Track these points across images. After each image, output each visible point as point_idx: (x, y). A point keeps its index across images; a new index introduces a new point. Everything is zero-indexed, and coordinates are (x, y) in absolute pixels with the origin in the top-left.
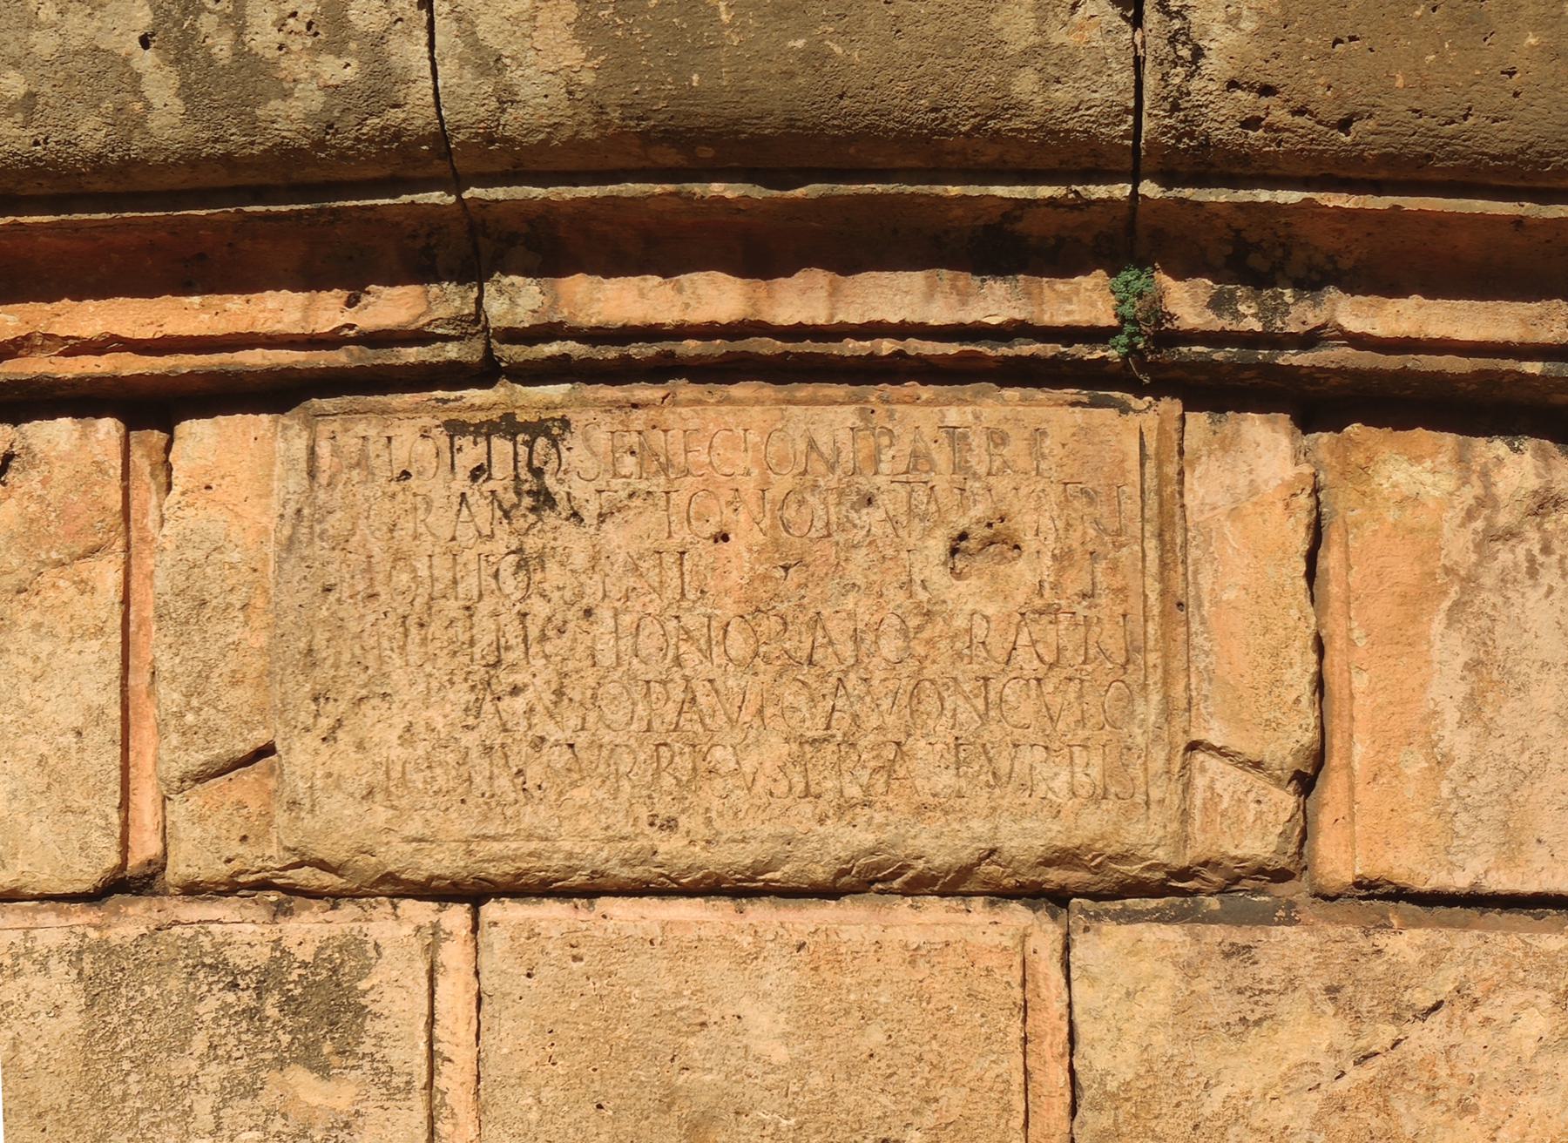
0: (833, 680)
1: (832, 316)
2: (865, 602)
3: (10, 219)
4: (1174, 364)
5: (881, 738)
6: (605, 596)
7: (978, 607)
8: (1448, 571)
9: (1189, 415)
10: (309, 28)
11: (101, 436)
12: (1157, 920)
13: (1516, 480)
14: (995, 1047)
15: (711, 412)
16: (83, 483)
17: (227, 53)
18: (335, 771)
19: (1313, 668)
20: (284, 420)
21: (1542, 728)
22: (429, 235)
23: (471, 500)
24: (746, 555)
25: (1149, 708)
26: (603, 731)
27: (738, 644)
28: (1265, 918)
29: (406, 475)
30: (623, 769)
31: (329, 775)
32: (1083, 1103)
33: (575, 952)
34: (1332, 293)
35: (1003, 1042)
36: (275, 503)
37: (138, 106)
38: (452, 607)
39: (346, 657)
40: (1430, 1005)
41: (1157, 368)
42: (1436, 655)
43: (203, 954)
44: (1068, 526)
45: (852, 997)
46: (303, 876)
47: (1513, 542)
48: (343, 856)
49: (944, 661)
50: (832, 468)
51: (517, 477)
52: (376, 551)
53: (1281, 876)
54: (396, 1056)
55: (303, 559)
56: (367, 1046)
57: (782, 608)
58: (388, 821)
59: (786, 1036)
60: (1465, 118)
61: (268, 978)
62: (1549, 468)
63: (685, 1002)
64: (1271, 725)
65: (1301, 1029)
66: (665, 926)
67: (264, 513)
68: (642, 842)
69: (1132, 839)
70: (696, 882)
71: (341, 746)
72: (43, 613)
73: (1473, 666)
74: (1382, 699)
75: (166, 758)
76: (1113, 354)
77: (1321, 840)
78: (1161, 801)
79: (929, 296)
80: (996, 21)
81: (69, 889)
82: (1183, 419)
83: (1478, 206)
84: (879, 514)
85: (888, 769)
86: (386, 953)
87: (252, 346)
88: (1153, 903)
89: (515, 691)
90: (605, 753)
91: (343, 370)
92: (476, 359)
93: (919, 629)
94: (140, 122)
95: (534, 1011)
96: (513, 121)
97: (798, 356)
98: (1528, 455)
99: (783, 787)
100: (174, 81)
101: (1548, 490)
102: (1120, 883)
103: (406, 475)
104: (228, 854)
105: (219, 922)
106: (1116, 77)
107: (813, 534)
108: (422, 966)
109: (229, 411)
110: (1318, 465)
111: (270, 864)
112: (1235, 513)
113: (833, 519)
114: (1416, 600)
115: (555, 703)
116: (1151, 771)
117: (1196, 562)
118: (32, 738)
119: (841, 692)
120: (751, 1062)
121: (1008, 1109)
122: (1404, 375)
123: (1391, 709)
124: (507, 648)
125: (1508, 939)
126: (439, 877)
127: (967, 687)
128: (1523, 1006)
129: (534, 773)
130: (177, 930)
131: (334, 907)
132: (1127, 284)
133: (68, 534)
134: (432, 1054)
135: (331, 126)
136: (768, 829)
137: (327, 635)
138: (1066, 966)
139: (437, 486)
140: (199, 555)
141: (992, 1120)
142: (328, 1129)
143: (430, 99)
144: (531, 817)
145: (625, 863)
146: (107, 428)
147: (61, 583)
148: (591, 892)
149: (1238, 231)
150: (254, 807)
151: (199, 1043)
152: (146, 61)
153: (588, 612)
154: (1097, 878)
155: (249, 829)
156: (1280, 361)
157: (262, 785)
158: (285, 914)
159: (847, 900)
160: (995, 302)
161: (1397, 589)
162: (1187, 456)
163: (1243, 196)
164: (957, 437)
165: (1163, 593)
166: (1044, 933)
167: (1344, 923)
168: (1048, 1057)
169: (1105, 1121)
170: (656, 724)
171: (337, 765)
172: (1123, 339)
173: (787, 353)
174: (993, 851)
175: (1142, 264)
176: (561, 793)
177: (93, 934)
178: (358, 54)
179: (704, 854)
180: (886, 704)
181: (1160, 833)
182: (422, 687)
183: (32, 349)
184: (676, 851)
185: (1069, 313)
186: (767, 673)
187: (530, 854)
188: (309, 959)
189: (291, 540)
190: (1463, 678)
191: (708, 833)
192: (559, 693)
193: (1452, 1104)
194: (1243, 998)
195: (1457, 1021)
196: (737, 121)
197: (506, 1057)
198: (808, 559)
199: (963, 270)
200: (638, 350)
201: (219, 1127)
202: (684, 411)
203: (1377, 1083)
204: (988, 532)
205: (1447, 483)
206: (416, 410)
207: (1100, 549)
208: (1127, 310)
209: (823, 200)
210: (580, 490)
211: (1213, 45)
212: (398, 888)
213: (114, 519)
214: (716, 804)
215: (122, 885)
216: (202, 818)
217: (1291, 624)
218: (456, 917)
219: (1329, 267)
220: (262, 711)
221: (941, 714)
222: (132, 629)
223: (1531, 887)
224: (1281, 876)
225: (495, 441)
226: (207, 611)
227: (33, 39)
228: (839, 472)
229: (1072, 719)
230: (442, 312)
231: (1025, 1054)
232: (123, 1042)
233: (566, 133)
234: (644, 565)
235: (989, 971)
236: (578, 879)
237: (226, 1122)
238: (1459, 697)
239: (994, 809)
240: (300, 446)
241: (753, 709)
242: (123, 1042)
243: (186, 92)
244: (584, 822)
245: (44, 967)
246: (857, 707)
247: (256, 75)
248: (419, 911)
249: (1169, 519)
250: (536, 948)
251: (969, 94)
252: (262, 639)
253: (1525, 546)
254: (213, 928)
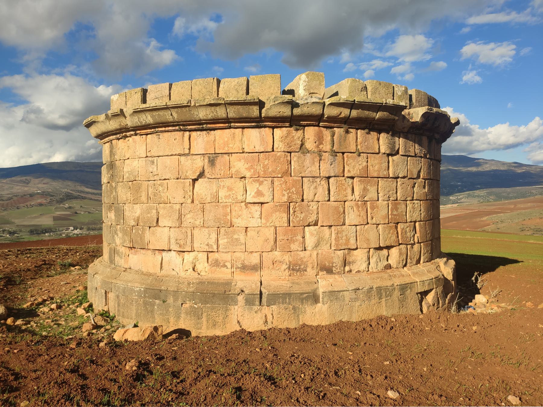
41: (181, 130)
160: (174, 128)
215: (147, 157)
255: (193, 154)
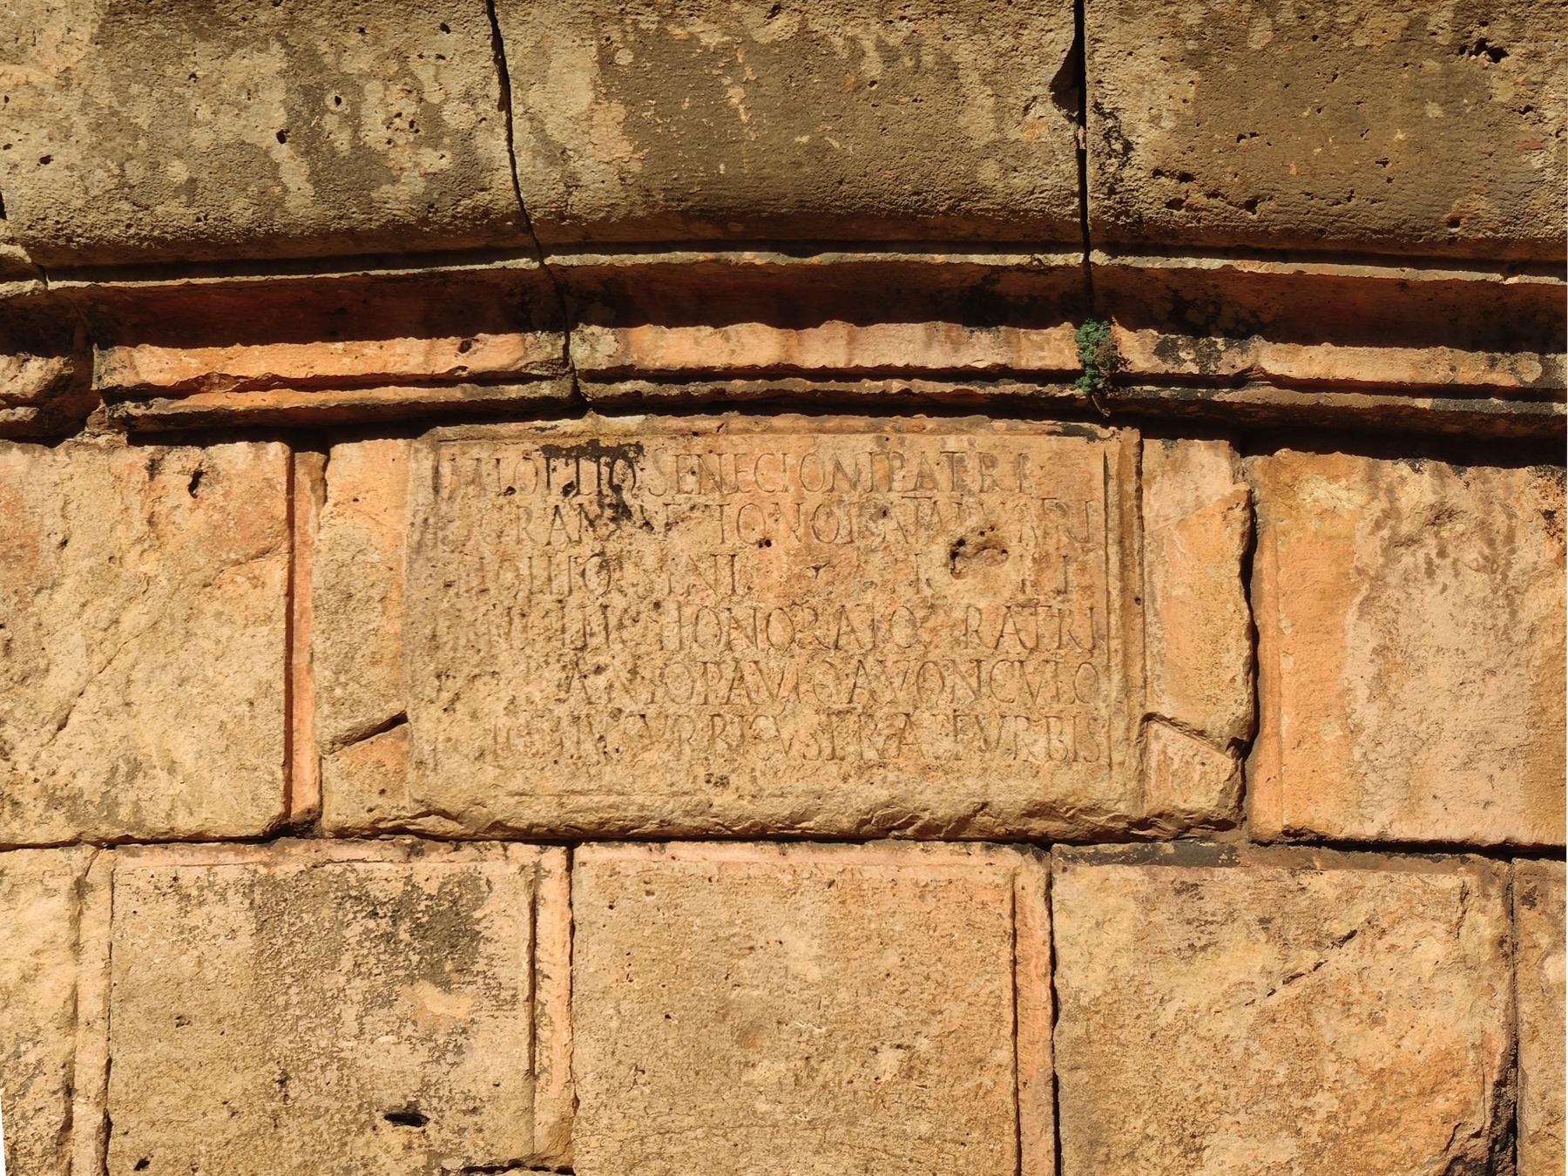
0: (854, 662)
1: (850, 361)
2: (882, 597)
3: (185, 280)
4: (1130, 401)
5: (893, 710)
6: (671, 591)
7: (973, 602)
8: (1360, 571)
9: (1147, 442)
10: (411, 125)
11: (270, 457)
12: (1123, 862)
13: (1416, 496)
14: (989, 969)
15: (757, 440)
16: (257, 496)
17: (346, 146)
18: (453, 736)
19: (1246, 653)
20: (416, 444)
21: (1438, 703)
22: (523, 294)
23: (563, 512)
24: (785, 558)
25: (1112, 686)
26: (669, 704)
27: (778, 632)
28: (1211, 861)
29: (511, 490)
30: (685, 736)
31: (449, 740)
32: (1061, 1015)
33: (648, 887)
34: (1257, 342)
35: (995, 964)
36: (408, 512)
37: (277, 190)
38: (547, 601)
39: (463, 641)
40: (1345, 934)
42: (1349, 641)
43: (349, 888)
44: (1046, 534)
45: (873, 926)
46: (430, 823)
47: (1415, 547)
48: (460, 807)
49: (944, 647)
50: (854, 486)
51: (600, 492)
52: (487, 554)
53: (1224, 825)
54: (504, 974)
55: (429, 560)
56: (481, 965)
57: (814, 601)
58: (495, 778)
59: (819, 958)
60: (1349, 199)
61: (401, 908)
62: (1443, 486)
63: (737, 930)
64: (1212, 700)
65: (1239, 954)
66: (721, 866)
67: (400, 521)
68: (700, 797)
69: (1098, 795)
70: (747, 830)
71: (459, 715)
72: (224, 604)
73: (1381, 651)
74: (1304, 678)
75: (320, 724)
76: (1079, 392)
77: (1256, 795)
78: (1122, 764)
79: (928, 345)
80: (963, 121)
81: (243, 833)
82: (1141, 445)
83: (1368, 271)
84: (893, 524)
85: (900, 736)
86: (496, 888)
87: (386, 384)
88: (1119, 848)
89: (599, 670)
90: (670, 722)
91: (459, 404)
92: (565, 395)
93: (925, 619)
94: (279, 203)
95: (615, 937)
96: (578, 201)
97: (825, 393)
98: (1426, 475)
99: (814, 751)
100: (305, 169)
101: (1442, 504)
102: (1091, 831)
103: (511, 490)
104: (369, 805)
105: (363, 861)
106: (1062, 167)
107: (839, 541)
108: (524, 900)
109: (373, 436)
110: (1254, 484)
111: (404, 813)
112: (1182, 524)
113: (855, 528)
114: (1333, 596)
115: (631, 681)
116: (1113, 739)
117: (1151, 564)
118: (214, 707)
119: (861, 672)
120: (790, 980)
121: (999, 1019)
122: (1317, 409)
123: (1312, 686)
124: (592, 635)
125: (1410, 879)
126: (538, 825)
127: (963, 668)
128: (1423, 935)
129: (613, 739)
130: (329, 867)
131: (457, 849)
132: (1087, 334)
133: (244, 538)
134: (533, 972)
135: (432, 206)
136: (801, 786)
137: (448, 623)
138: (1049, 900)
139: (535, 499)
140: (347, 556)
141: (986, 1029)
142: (449, 1035)
143: (510, 184)
144: (611, 775)
145: (687, 813)
146: (276, 451)
147: (238, 579)
148: (662, 836)
149: (1176, 292)
150: (390, 765)
151: (346, 962)
152: (282, 152)
153: (657, 605)
154: (1072, 827)
155: (387, 784)
156: (1215, 398)
157: (398, 747)
158: (417, 854)
159: (870, 845)
160: (981, 349)
161: (1317, 586)
162: (1145, 476)
163: (1174, 263)
164: (954, 461)
165: (1123, 590)
166: (1030, 873)
167: (1276, 865)
168: (1034, 977)
169: (1079, 1030)
170: (711, 698)
171: (455, 732)
172: (1086, 380)
173: (816, 391)
174: (985, 805)
175: (1101, 317)
176: (635, 756)
177: (263, 871)
178: (451, 147)
179: (751, 807)
180: (897, 682)
181: (1121, 790)
182: (523, 667)
183: (212, 386)
184: (727, 804)
185: (1042, 358)
186: (801, 656)
187: (610, 806)
188: (434, 893)
189: (420, 544)
190: (1372, 661)
191: (754, 790)
192: (634, 672)
193: (1364, 1017)
194: (1191, 928)
195: (1368, 948)
196: (758, 202)
197: (592, 975)
198: (835, 561)
199: (956, 322)
200: (696, 388)
201: (362, 1032)
202: (734, 438)
203: (1302, 999)
204: (981, 539)
205: (1360, 498)
206: (520, 437)
207: (1072, 554)
208: (1088, 357)
209: (834, 267)
210: (652, 504)
211: (1140, 140)
212: (509, 834)
213: (281, 526)
214: (760, 765)
215: (289, 829)
216: (349, 775)
217: (1228, 616)
218: (554, 858)
219: (1253, 320)
220: (396, 686)
221: (942, 690)
222: (296, 617)
223: (1428, 835)
224: (1224, 825)
225: (583, 462)
226: (353, 603)
227: (193, 135)
228: (860, 489)
229: (1048, 695)
230: (536, 356)
231: (1014, 974)
232: (286, 960)
233: (622, 212)
234: (702, 566)
235: (984, 904)
236: (650, 827)
237: (367, 1028)
238: (1368, 677)
239: (985, 770)
240: (428, 464)
241: (790, 686)
242: (286, 960)
243: (315, 178)
244: (654, 780)
245: (223, 897)
246: (874, 684)
247: (369, 166)
248: (524, 853)
249: (1129, 526)
250: (617, 885)
251: (942, 181)
252: (397, 626)
253: (1424, 550)
254: (358, 866)
255: (1306, 842)
